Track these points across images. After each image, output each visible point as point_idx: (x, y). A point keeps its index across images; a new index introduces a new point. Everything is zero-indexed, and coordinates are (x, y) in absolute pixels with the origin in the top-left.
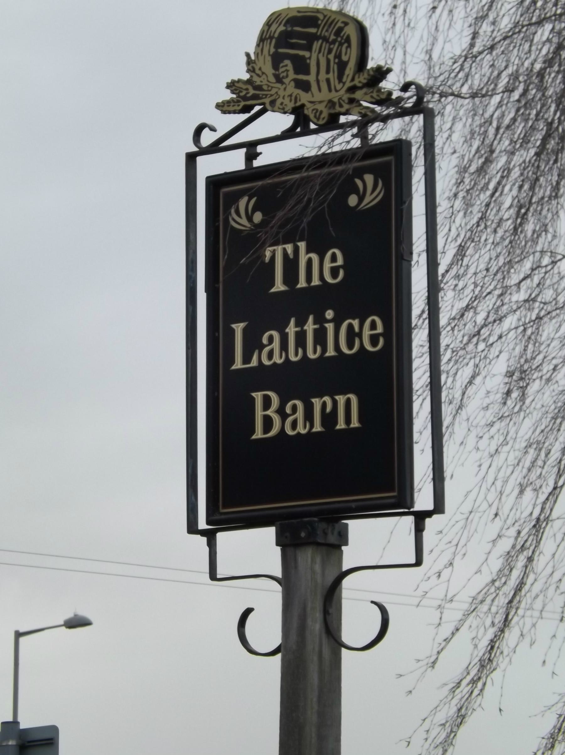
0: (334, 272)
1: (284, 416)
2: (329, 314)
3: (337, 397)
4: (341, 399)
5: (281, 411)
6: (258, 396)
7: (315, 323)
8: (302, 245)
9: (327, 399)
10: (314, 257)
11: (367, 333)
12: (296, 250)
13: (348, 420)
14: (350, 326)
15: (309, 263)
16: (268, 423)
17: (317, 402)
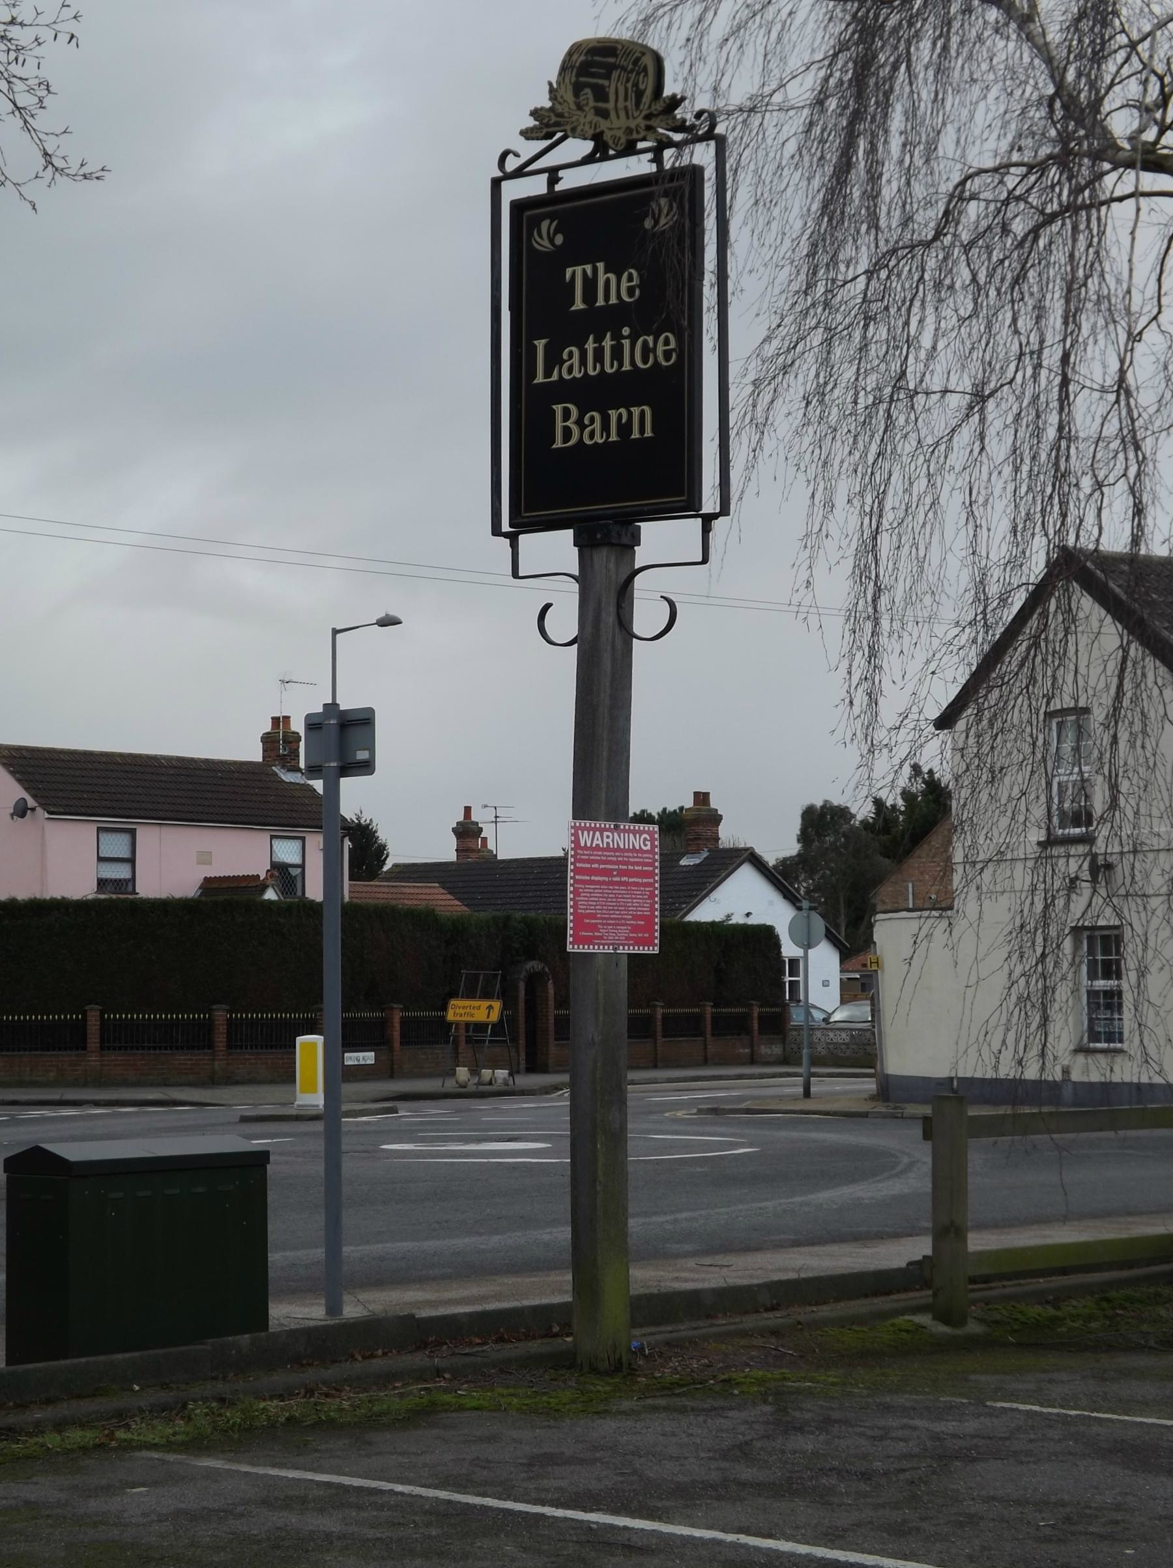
0: (630, 292)
1: (582, 426)
2: (626, 331)
3: (632, 409)
4: (636, 411)
5: (580, 423)
6: (558, 408)
7: (612, 340)
8: (601, 266)
9: (623, 411)
10: (612, 277)
11: (661, 348)
12: (595, 270)
13: (642, 430)
14: (645, 343)
15: (608, 282)
16: (567, 433)
17: (613, 414)
